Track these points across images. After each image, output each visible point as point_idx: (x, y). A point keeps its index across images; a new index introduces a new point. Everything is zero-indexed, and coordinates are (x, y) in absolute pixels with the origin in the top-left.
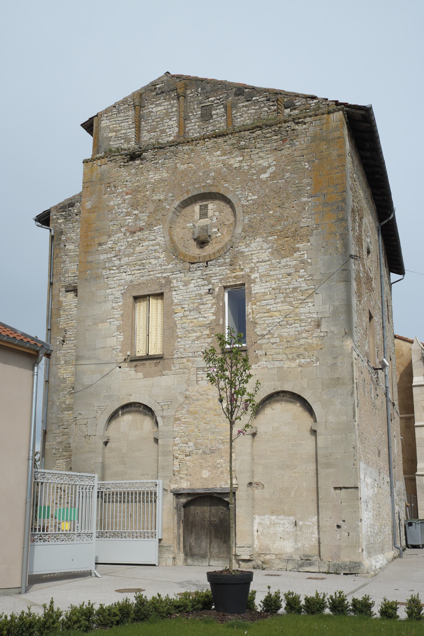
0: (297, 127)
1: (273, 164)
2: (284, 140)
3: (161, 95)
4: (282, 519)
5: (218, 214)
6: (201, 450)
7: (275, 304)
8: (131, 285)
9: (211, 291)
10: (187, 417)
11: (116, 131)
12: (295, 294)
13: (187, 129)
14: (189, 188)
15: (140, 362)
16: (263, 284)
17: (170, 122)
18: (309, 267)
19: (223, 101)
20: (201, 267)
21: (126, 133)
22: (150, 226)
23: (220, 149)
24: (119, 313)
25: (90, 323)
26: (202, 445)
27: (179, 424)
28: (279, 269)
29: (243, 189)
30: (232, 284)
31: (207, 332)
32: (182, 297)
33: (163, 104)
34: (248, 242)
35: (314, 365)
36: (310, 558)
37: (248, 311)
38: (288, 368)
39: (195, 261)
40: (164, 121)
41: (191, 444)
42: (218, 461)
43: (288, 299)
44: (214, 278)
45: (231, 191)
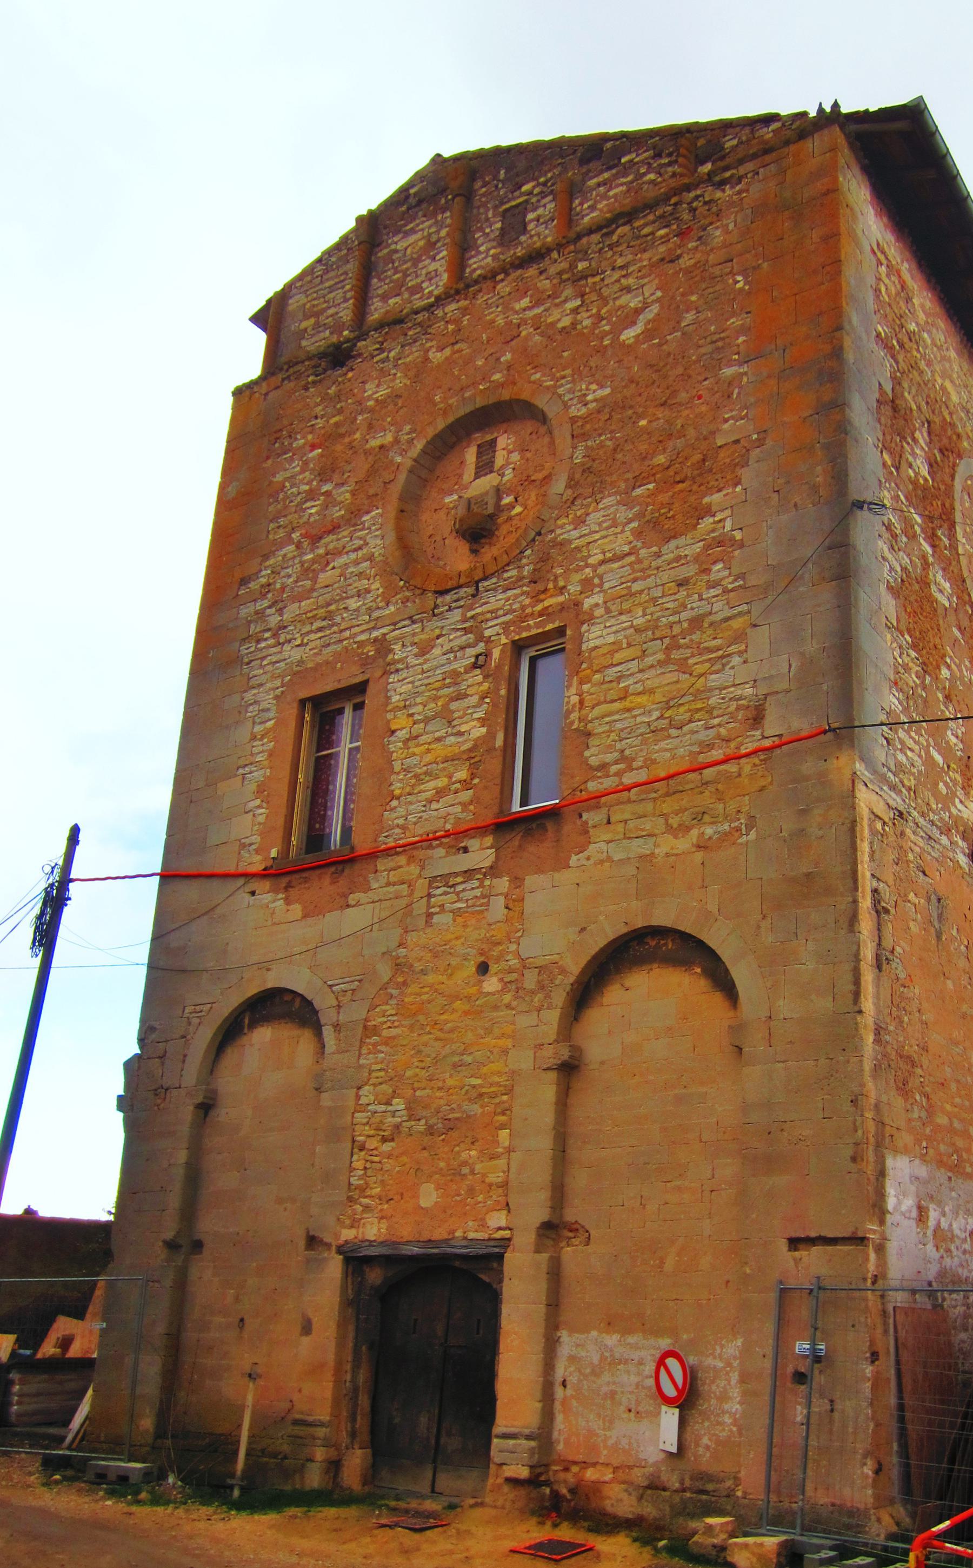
0: (719, 194)
1: (654, 297)
2: (682, 234)
3: (416, 209)
4: (636, 1347)
5: (519, 458)
6: (423, 1122)
7: (641, 671)
8: (300, 673)
9: (481, 658)
10: (396, 1024)
11: (317, 315)
12: (693, 637)
13: (468, 270)
14: (450, 401)
15: (297, 876)
16: (613, 621)
17: (433, 264)
18: (737, 553)
19: (553, 185)
20: (462, 598)
21: (337, 313)
22: (354, 515)
23: (529, 293)
24: (265, 748)
25: (201, 784)
26: (426, 1107)
27: (375, 1045)
28: (655, 572)
29: (578, 375)
30: (535, 631)
31: (462, 774)
32: (410, 685)
33: (421, 227)
34: (579, 513)
35: (740, 841)
36: (710, 1487)
37: (568, 703)
38: (667, 855)
39: (450, 584)
40: (420, 265)
41: (399, 1104)
42: (464, 1155)
43: (675, 655)
44: (490, 624)
45: (548, 388)
